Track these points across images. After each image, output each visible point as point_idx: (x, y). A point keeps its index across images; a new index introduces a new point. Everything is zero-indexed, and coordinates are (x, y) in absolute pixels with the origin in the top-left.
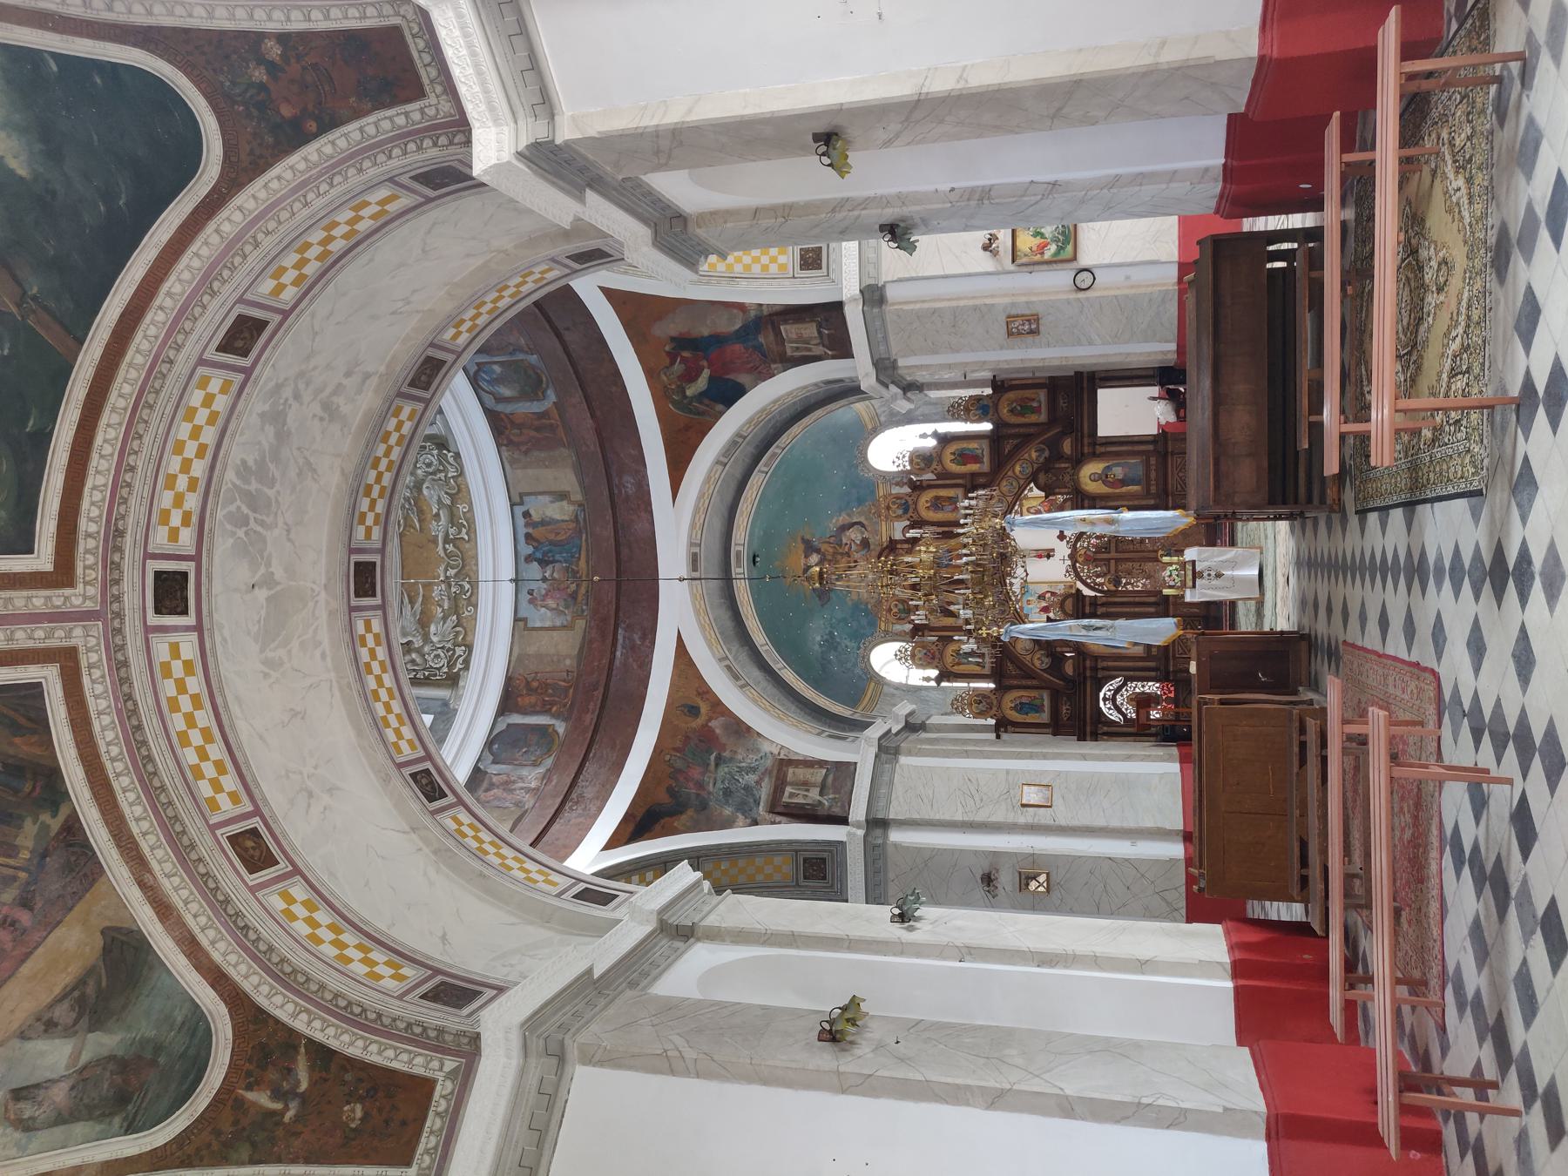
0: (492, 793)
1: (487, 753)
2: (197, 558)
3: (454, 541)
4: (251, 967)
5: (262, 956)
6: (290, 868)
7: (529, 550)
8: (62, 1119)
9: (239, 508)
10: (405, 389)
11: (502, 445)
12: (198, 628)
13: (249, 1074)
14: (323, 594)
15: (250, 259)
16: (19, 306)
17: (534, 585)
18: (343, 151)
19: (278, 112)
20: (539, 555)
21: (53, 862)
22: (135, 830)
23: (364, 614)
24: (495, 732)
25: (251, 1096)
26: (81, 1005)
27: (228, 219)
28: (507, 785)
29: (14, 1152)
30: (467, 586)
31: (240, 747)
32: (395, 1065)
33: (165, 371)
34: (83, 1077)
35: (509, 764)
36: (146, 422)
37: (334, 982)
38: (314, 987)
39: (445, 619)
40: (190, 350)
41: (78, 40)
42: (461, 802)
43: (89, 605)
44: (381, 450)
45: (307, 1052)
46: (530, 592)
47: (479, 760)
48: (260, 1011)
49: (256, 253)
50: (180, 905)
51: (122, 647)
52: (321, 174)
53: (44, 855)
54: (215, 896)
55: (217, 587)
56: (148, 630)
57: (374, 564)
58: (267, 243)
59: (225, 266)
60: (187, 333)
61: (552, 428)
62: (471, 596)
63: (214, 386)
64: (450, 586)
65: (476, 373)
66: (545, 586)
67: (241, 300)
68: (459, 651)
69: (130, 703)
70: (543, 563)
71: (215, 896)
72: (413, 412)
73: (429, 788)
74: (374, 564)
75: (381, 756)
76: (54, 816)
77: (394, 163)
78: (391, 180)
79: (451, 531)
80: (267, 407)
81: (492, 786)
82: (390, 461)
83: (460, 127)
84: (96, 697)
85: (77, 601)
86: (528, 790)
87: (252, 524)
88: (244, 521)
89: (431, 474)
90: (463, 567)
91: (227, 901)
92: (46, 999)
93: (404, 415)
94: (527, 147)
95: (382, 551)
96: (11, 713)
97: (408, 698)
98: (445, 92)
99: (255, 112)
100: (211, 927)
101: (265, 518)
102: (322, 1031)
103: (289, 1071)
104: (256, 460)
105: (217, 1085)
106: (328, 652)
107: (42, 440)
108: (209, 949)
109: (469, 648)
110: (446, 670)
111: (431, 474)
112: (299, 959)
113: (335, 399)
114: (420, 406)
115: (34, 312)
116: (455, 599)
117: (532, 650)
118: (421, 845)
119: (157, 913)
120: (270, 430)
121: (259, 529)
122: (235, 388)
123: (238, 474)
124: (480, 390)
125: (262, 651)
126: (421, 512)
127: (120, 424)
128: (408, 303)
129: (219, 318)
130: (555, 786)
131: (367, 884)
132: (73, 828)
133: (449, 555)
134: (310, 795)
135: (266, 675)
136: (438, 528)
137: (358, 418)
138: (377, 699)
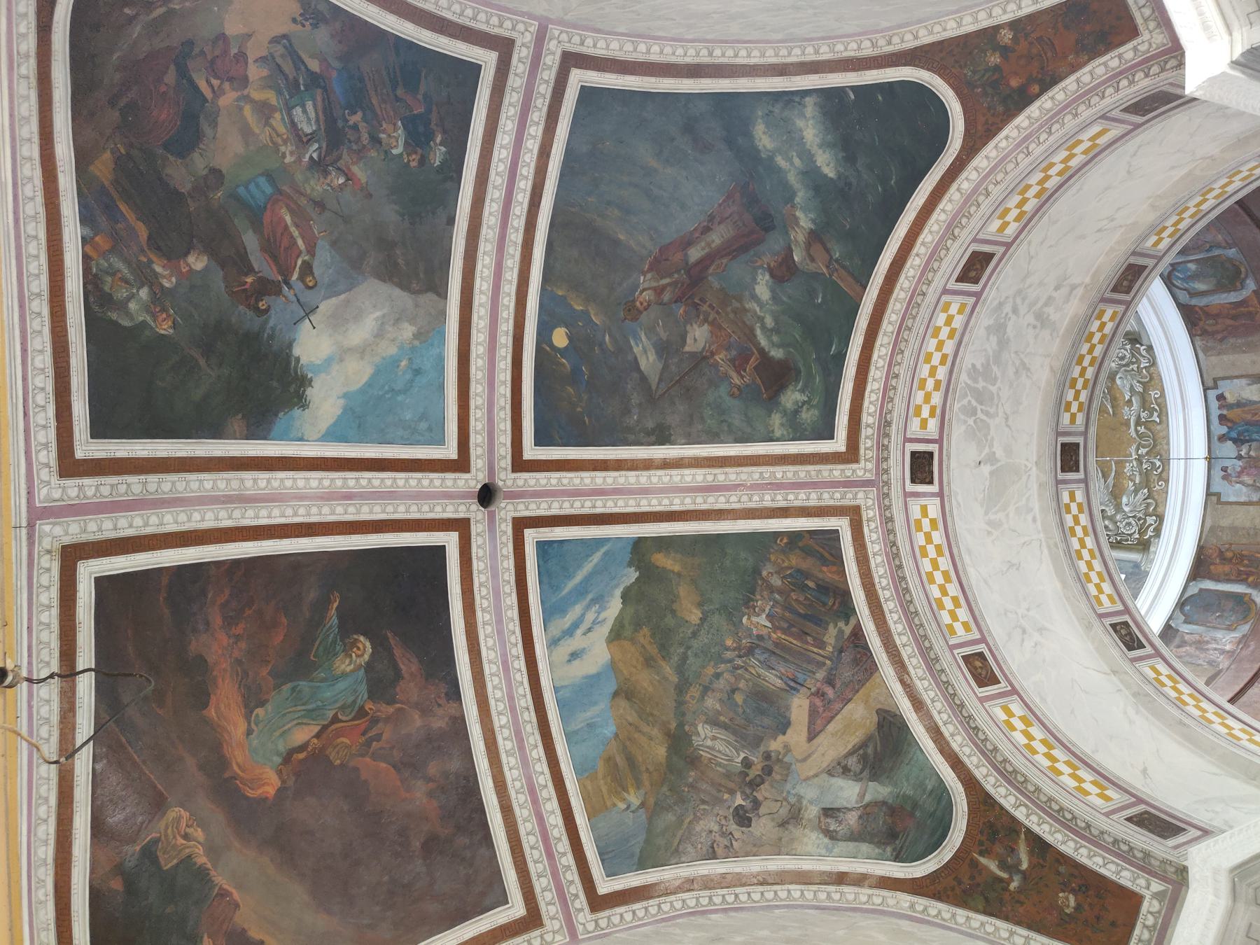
0: (1184, 649)
1: (1178, 613)
2: (939, 441)
3: (1146, 424)
4: (980, 760)
5: (989, 753)
6: (1009, 688)
7: (1224, 430)
8: (854, 837)
9: (969, 401)
10: (1108, 295)
11: (1195, 335)
12: (941, 494)
13: (981, 843)
14: (1034, 469)
15: (982, 207)
16: (827, 267)
17: (1227, 463)
18: (1060, 103)
19: (1008, 85)
20: (1234, 435)
21: (847, 657)
22: (898, 642)
23: (1068, 486)
24: (1186, 595)
25: (983, 860)
26: (864, 759)
27: (967, 179)
28: (1200, 644)
29: (823, 852)
30: (1158, 463)
31: (971, 587)
32: (1103, 871)
33: (919, 302)
34: (868, 811)
35: (1202, 625)
36: (906, 341)
37: (1048, 788)
38: (1032, 788)
39: (1136, 492)
40: (938, 283)
41: (868, 73)
42: (1158, 654)
43: (868, 476)
44: (1085, 348)
45: (1026, 839)
46: (1224, 469)
47: (1170, 618)
48: (988, 796)
49: (987, 201)
50: (929, 702)
51: (889, 507)
52: (1041, 126)
53: (841, 651)
54: (953, 700)
55: (953, 464)
56: (907, 495)
57: (1077, 445)
58: (996, 191)
59: (964, 215)
60: (935, 271)
61: (1251, 315)
62: (1162, 472)
63: (954, 309)
64: (1141, 463)
65: (1170, 274)
66: (1240, 463)
67: (975, 240)
68: (1150, 520)
69: (894, 548)
70: (1238, 441)
71: (953, 700)
72: (1115, 313)
73: (1128, 638)
74: (1077, 445)
75: (1084, 606)
76: (846, 625)
77: (1107, 101)
78: (1104, 117)
79: (1143, 415)
80: (991, 322)
81: (1183, 643)
82: (937, 337)
83: (1174, 52)
84: (872, 542)
85: (860, 473)
86: (1223, 652)
87: (980, 415)
88: (973, 412)
89: (1124, 366)
90: (1155, 446)
91: (962, 705)
92: (843, 750)
93: (1106, 318)
94: (1243, 54)
95: (1085, 434)
96: (821, 550)
97: (1107, 558)
98: (1159, 26)
99: (990, 90)
100: (950, 723)
101: (988, 409)
102: (1039, 825)
103: (1012, 850)
104: (982, 364)
105: (958, 845)
106: (1038, 517)
107: (841, 358)
108: (949, 739)
109: (1160, 518)
110: (1137, 536)
111: (1124, 366)
112: (1018, 762)
113: (1046, 310)
114: (1121, 308)
115: (837, 270)
116: (1146, 475)
117: (1225, 523)
118: (1121, 687)
119: (913, 705)
120: (994, 339)
121: (984, 417)
122: (968, 310)
123: (969, 375)
124: (1174, 288)
125: (986, 513)
126: (1114, 400)
127: (889, 344)
128: (1112, 220)
129: (958, 256)
130: (1253, 652)
131: (1072, 712)
132: (858, 633)
133: (1140, 436)
134: (1024, 632)
135: (989, 533)
136: (1131, 413)
137: (1066, 323)
138: (1080, 558)
